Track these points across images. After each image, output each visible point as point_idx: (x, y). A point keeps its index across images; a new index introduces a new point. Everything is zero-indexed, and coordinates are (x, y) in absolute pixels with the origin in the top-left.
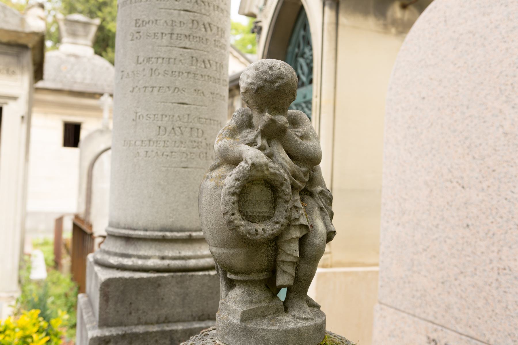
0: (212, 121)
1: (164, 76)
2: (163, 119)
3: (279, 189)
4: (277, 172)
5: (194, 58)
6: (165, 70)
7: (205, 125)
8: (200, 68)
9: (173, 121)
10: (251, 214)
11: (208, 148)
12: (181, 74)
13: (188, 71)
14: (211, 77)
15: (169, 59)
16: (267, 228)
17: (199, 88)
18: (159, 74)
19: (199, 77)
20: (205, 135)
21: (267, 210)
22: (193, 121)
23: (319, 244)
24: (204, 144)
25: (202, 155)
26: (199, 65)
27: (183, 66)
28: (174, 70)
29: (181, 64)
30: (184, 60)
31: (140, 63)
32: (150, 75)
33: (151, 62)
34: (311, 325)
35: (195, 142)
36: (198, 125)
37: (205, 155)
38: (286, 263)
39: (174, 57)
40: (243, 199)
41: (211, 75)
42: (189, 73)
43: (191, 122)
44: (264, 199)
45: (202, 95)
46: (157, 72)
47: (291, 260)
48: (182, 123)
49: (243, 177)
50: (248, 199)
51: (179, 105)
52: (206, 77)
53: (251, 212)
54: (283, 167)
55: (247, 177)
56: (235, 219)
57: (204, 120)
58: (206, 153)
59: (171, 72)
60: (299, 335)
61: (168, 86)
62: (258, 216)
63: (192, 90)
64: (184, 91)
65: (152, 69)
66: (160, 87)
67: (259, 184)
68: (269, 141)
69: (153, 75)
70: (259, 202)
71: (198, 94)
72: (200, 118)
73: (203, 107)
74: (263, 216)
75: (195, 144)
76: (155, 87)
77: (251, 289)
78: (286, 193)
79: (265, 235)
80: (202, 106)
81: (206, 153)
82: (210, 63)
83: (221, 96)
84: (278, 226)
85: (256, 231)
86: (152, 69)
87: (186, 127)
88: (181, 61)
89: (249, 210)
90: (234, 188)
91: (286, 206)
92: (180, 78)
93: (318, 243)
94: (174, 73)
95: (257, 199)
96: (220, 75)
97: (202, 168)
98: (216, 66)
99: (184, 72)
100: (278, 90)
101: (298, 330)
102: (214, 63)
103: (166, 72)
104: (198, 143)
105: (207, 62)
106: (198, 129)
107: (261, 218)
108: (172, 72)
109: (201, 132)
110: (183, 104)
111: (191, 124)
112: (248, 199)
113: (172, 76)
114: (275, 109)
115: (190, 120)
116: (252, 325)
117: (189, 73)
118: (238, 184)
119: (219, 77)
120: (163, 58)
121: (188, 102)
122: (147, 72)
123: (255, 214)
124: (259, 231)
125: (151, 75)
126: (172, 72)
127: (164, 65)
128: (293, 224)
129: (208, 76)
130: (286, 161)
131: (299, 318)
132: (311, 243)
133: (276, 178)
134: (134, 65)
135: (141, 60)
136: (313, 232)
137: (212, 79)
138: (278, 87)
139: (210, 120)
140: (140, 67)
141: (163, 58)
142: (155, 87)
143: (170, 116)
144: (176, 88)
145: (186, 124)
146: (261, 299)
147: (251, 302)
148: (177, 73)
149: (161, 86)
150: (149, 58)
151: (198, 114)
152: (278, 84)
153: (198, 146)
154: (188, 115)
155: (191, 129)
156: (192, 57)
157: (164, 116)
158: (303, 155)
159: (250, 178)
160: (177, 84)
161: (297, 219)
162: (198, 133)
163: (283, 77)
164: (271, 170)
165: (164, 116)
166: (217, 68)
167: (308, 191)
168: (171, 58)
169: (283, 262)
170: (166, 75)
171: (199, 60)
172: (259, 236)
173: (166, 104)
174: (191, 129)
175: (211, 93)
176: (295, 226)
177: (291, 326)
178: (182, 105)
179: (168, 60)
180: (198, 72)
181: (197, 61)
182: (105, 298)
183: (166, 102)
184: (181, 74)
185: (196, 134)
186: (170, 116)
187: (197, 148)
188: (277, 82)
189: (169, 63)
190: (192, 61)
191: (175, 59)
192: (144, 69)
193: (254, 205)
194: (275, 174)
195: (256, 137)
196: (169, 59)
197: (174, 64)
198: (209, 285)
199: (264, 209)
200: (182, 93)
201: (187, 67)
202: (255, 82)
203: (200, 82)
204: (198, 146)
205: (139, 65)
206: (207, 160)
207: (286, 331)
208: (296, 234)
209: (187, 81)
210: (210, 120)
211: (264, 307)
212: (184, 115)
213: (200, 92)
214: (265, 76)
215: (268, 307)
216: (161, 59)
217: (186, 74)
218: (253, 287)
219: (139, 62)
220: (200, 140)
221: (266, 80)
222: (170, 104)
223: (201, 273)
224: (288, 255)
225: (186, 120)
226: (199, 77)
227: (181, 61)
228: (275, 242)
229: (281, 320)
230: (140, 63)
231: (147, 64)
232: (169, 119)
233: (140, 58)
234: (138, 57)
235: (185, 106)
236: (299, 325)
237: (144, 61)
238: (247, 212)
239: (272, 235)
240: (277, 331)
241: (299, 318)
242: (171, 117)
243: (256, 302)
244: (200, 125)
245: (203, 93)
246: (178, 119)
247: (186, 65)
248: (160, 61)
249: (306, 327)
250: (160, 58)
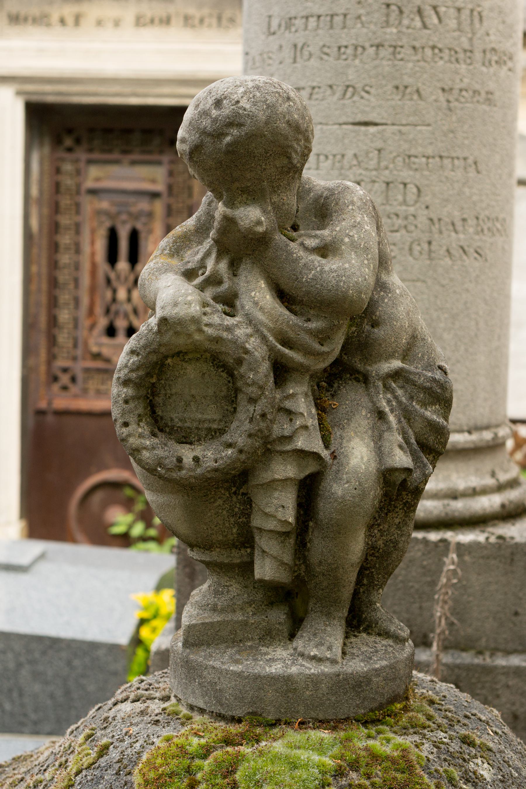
0: (446, 162)
1: (321, 59)
2: (321, 165)
3: (236, 373)
4: (225, 335)
5: (393, 8)
6: (324, 46)
7: (426, 173)
8: (410, 31)
9: (342, 168)
10: (180, 424)
11: (435, 229)
12: (360, 50)
13: (377, 42)
14: (440, 50)
15: (332, 16)
16: (204, 456)
17: (407, 80)
18: (311, 55)
19: (407, 52)
20: (427, 199)
21: (217, 417)
22: (391, 166)
23: (343, 497)
24: (422, 220)
25: (416, 248)
26: (406, 22)
27: (365, 30)
28: (345, 43)
29: (359, 25)
30: (368, 14)
31: (274, 33)
32: (291, 60)
33: (293, 29)
34: (323, 674)
35: (397, 215)
36: (406, 174)
37: (426, 246)
38: (265, 534)
39: (343, 11)
40: (163, 392)
41: (440, 46)
42: (378, 46)
43: (387, 168)
44: (210, 392)
45: (415, 97)
46: (306, 53)
47: (272, 528)
48: (364, 172)
49: (145, 347)
50: (174, 391)
51: (357, 128)
52: (428, 52)
53: (181, 420)
54: (250, 322)
55: (154, 346)
56: (129, 435)
57: (424, 160)
58: (430, 243)
59: (336, 49)
60: (289, 691)
61: (330, 83)
62: (197, 428)
63: (389, 87)
64: (368, 92)
65: (295, 46)
66: (313, 88)
67: (198, 359)
68: (234, 266)
69: (298, 59)
70: (198, 398)
71: (404, 95)
72: (409, 157)
73: (419, 128)
74: (209, 430)
75: (399, 222)
76: (303, 88)
77: (223, 582)
78: (249, 381)
79: (199, 471)
80: (416, 125)
81: (430, 243)
82: (437, 13)
83: (476, 92)
84: (230, 452)
85: (180, 460)
86: (295, 46)
87: (374, 182)
88: (359, 17)
89: (175, 415)
90: (126, 371)
91: (252, 409)
92: (357, 62)
93: (340, 493)
94: (343, 50)
95: (193, 392)
96: (471, 40)
97: (418, 280)
98: (458, 18)
99: (367, 45)
100: (232, 150)
101: (287, 679)
102: (452, 12)
103: (326, 50)
104: (406, 218)
105: (429, 12)
106: (405, 185)
107: (203, 433)
108: (339, 48)
109: (415, 190)
110: (366, 124)
111: (387, 172)
112: (174, 391)
113: (338, 59)
114: (245, 191)
115: (383, 164)
116: (198, 657)
117: (378, 46)
118: (133, 363)
119: (467, 46)
120: (319, 17)
121: (377, 121)
122: (287, 54)
123: (188, 424)
124: (185, 460)
125: (295, 61)
126: (339, 48)
127: (320, 32)
128: (278, 448)
129: (433, 47)
130: (261, 309)
131: (302, 655)
132: (327, 494)
133: (223, 349)
134: (263, 37)
135: (275, 23)
136: (334, 468)
137: (446, 54)
138: (229, 145)
139: (441, 157)
140: (274, 42)
141: (319, 17)
142: (303, 88)
143: (334, 156)
144: (348, 87)
145: (374, 173)
146: (234, 604)
147: (214, 609)
148: (350, 51)
149: (315, 84)
150: (290, 19)
151: (406, 146)
152: (228, 139)
153: (405, 227)
154: (379, 151)
155: (388, 184)
156: (388, 6)
157: (322, 158)
158: (308, 293)
159: (163, 350)
160: (352, 76)
161: (289, 438)
162: (405, 194)
163: (242, 120)
164: (209, 331)
165: (322, 158)
166: (459, 24)
167: (359, 372)
168: (337, 15)
169: (260, 530)
170: (325, 57)
171: (406, 10)
172: (184, 472)
173: (325, 127)
174: (388, 184)
175: (443, 90)
176: (282, 453)
177: (276, 669)
178: (363, 128)
179: (328, 18)
180: (404, 41)
181: (401, 12)
182: (187, 570)
183: (327, 124)
184: (360, 50)
185: (400, 198)
186: (334, 156)
187: (403, 232)
188: (227, 134)
189: (331, 27)
190: (388, 15)
191: (345, 15)
192: (281, 47)
193: (187, 404)
194: (218, 340)
195: (207, 254)
196: (332, 16)
197: (344, 27)
198: (425, 563)
199: (211, 414)
200: (362, 98)
201: (374, 33)
202: (187, 136)
203: (410, 65)
204: (405, 227)
205: (271, 38)
206: (430, 259)
207: (257, 677)
208: (285, 470)
209: (376, 67)
210: (441, 157)
211: (237, 622)
212: (367, 153)
213: (408, 90)
214: (206, 123)
215: (245, 623)
216: (315, 19)
217: (372, 51)
218: (227, 578)
219: (272, 30)
220: (412, 210)
221: (204, 133)
222: (337, 127)
223: (466, 537)
224: (267, 515)
225: (373, 164)
226: (407, 52)
227: (359, 17)
228: (238, 482)
229: (266, 654)
230: (274, 33)
231: (287, 34)
232: (334, 164)
233: (273, 19)
234: (270, 17)
235: (372, 129)
236: (294, 670)
237: (280, 26)
238: (172, 420)
239: (216, 470)
240: (239, 675)
241: (302, 655)
242: (339, 157)
243: (223, 610)
244: (411, 173)
245: (418, 91)
246: (355, 162)
247: (372, 27)
248: (312, 22)
249: (309, 676)
250: (312, 16)
